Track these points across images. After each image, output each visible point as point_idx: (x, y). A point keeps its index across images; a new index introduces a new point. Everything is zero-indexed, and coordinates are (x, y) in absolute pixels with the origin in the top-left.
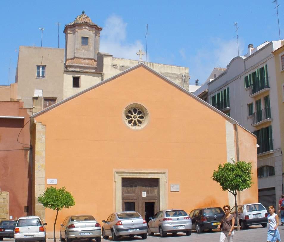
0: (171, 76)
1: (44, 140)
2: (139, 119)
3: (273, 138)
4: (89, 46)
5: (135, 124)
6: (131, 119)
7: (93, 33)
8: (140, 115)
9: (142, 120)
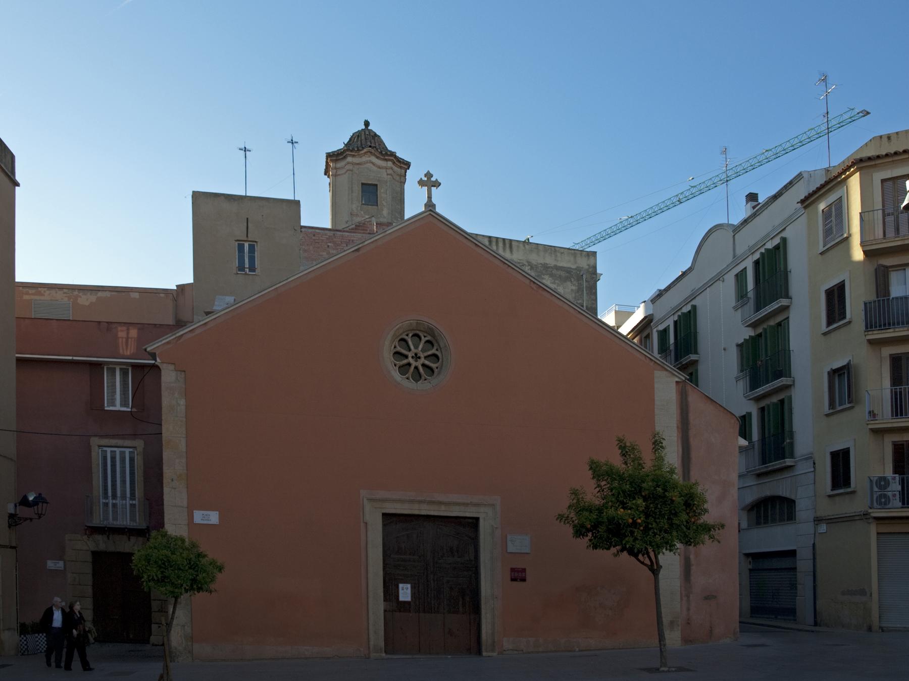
3: (795, 428)
4: (379, 207)
6: (405, 361)
7: (387, 174)
8: (430, 353)
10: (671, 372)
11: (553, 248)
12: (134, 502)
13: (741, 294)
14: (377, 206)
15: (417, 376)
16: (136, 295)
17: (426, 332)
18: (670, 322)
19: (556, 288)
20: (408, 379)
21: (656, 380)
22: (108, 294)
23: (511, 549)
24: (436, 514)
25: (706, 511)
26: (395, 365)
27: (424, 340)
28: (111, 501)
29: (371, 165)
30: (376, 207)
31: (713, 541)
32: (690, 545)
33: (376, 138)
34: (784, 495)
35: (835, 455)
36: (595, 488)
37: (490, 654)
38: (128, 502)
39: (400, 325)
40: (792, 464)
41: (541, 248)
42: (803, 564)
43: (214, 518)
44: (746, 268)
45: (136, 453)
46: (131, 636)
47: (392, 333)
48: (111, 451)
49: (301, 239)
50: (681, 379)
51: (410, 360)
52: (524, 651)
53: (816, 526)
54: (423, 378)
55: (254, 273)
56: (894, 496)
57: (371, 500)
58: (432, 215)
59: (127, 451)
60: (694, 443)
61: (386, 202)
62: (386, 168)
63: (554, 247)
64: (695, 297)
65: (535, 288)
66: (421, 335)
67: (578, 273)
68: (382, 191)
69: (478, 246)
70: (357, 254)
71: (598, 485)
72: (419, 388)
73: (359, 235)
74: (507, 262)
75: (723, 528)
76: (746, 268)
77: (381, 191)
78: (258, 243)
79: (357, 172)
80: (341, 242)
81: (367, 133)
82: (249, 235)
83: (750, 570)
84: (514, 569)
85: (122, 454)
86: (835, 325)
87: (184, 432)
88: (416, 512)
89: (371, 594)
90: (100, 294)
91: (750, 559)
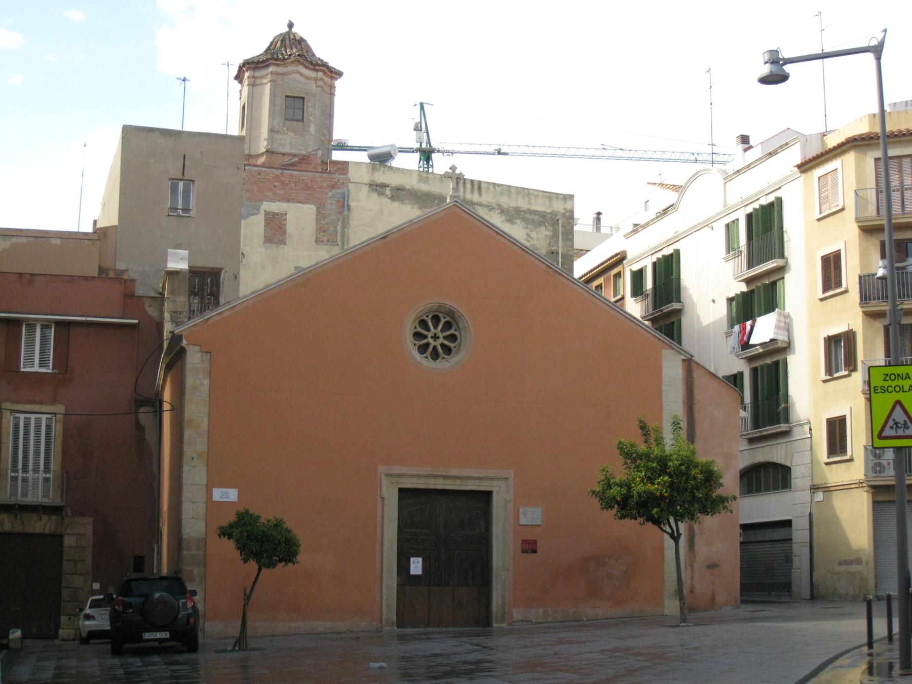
1: (207, 391)
2: (446, 342)
4: (306, 123)
6: (424, 341)
7: (317, 87)
8: (449, 333)
9: (451, 345)
10: (677, 351)
11: (526, 191)
12: (48, 476)
13: (731, 245)
14: (303, 121)
15: (435, 355)
16: (58, 242)
17: (446, 314)
18: (647, 264)
19: (529, 233)
22: (24, 240)
23: (523, 521)
24: (451, 488)
25: (721, 485)
26: (415, 345)
27: (443, 321)
28: (20, 475)
29: (298, 75)
30: (301, 123)
31: (726, 512)
32: (708, 515)
33: (303, 43)
34: (779, 462)
35: (826, 260)
36: (622, 466)
38: (41, 475)
39: (423, 307)
40: (788, 429)
41: (513, 190)
42: (800, 534)
43: (232, 495)
44: (737, 220)
45: (54, 419)
46: (34, 630)
47: (414, 315)
48: (25, 418)
49: (244, 178)
50: (686, 357)
51: (430, 340)
52: (534, 622)
53: (813, 494)
55: (188, 215)
56: (889, 464)
57: (388, 475)
58: (457, 206)
59: (44, 417)
60: (698, 416)
61: (314, 118)
62: (316, 79)
63: (528, 189)
64: (679, 240)
65: (551, 273)
66: (441, 316)
67: (554, 217)
68: (310, 105)
69: (499, 234)
70: (383, 241)
71: (625, 462)
72: (438, 367)
73: (311, 174)
74: (525, 249)
75: (735, 500)
76: (737, 220)
77: (309, 106)
78: (196, 183)
79: (281, 83)
80: (290, 181)
81: (292, 36)
82: (185, 174)
84: (525, 540)
85: (27, 420)
86: (831, 293)
87: (207, 412)
88: (432, 487)
89: (385, 567)
90: (14, 240)
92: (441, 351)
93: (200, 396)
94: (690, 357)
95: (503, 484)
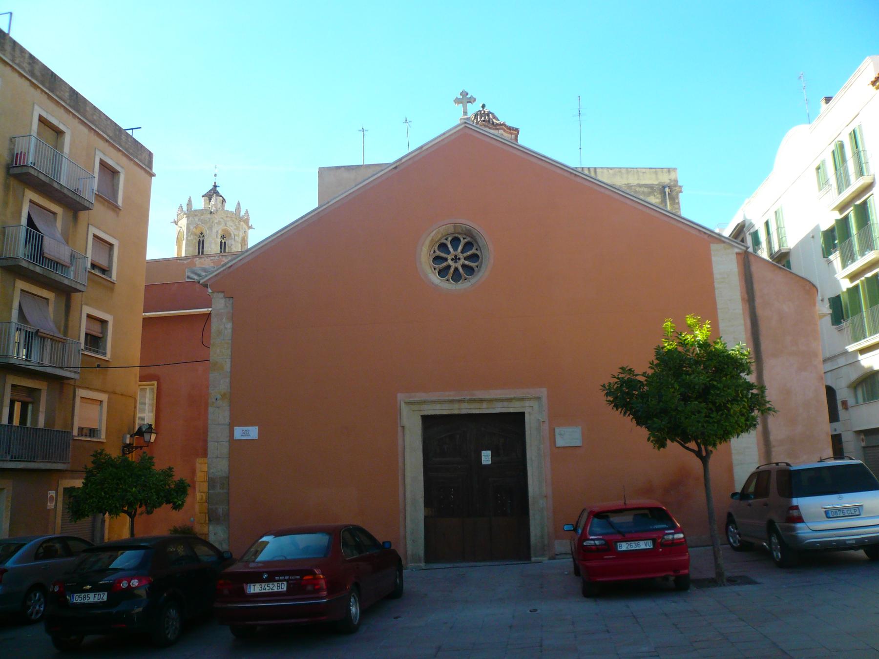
0: (637, 189)
2: (467, 263)
5: (457, 277)
6: (445, 264)
8: (469, 253)
17: (465, 234)
20: (448, 280)
21: (713, 253)
23: (560, 442)
24: (477, 412)
26: (435, 269)
27: (463, 242)
37: (539, 559)
43: (253, 432)
51: (450, 262)
54: (463, 278)
57: (409, 403)
83: (864, 447)
91: (862, 436)
92: (463, 272)
93: (223, 340)
94: (745, 249)
95: (535, 404)
